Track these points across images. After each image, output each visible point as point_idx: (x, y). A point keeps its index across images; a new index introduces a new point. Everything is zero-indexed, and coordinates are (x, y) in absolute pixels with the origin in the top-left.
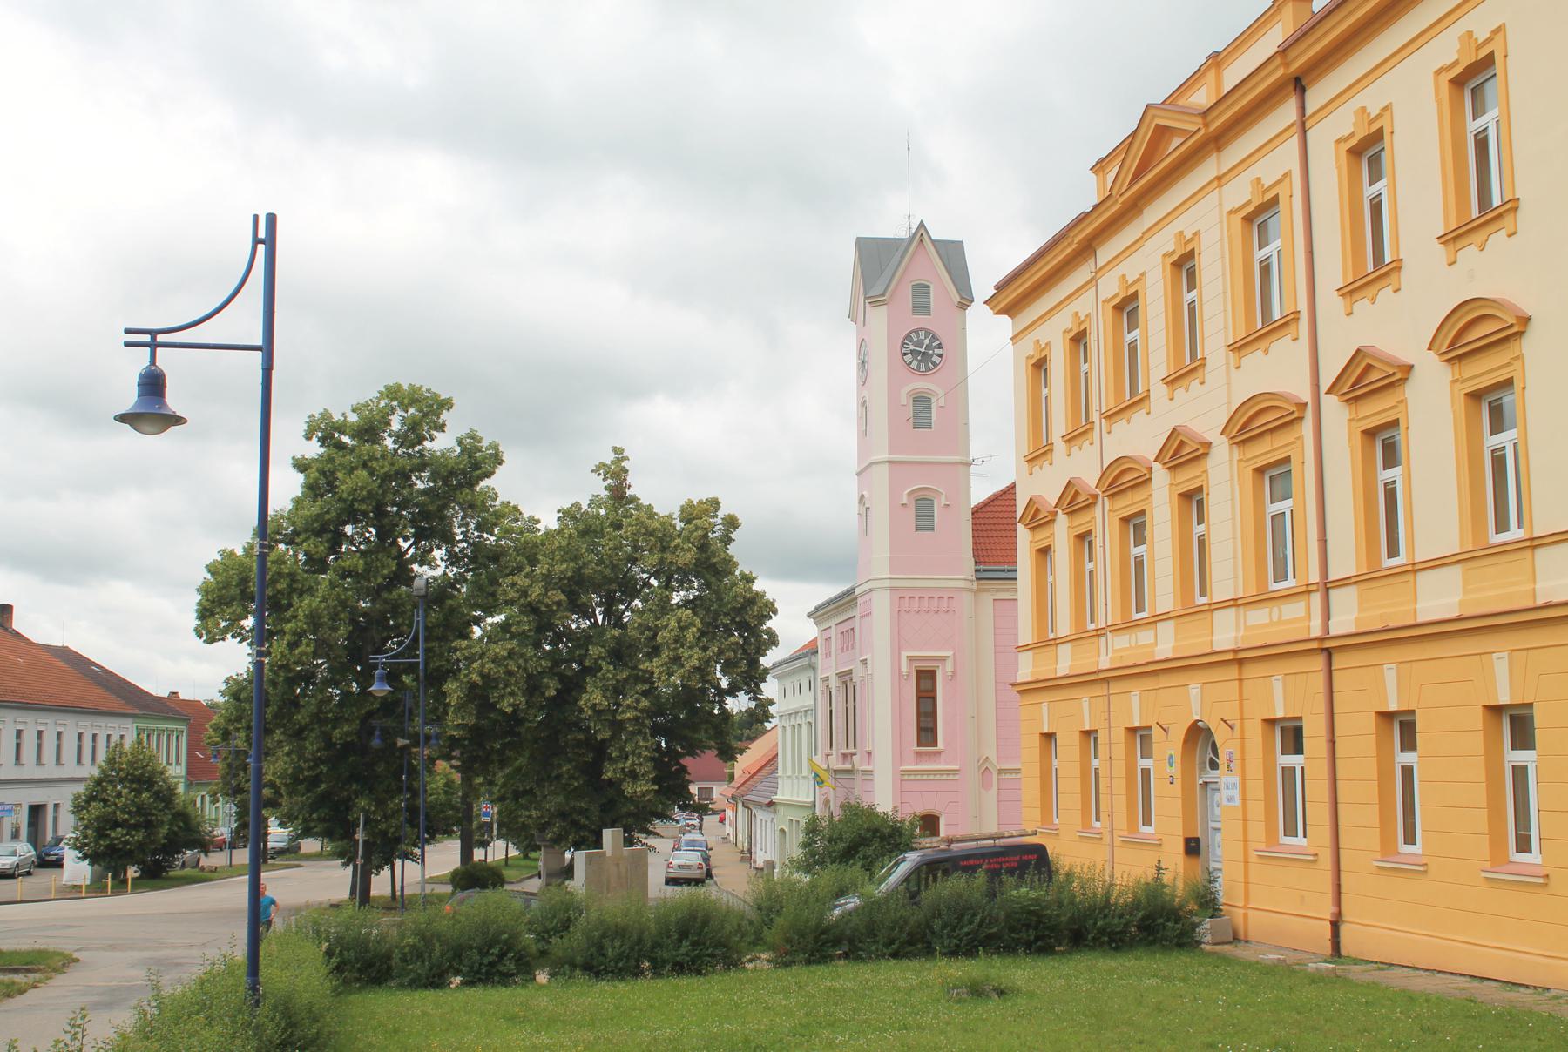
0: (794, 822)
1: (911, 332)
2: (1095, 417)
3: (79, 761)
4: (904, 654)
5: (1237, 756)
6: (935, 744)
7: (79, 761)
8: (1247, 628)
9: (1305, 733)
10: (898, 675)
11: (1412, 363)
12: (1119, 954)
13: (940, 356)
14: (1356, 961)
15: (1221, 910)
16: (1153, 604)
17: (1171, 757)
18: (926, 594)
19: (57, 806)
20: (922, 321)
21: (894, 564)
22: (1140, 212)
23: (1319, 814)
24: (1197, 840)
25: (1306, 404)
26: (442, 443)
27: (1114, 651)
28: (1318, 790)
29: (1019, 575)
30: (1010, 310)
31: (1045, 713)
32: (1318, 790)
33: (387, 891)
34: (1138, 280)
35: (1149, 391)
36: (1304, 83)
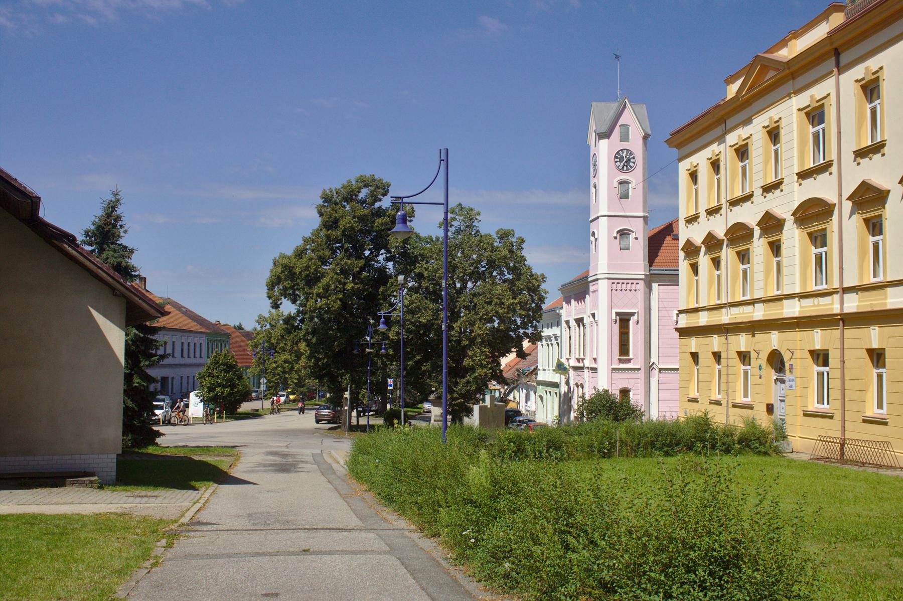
0: (548, 393)
1: (619, 151)
2: (723, 201)
3: (182, 356)
4: (614, 311)
5: (613, 323)
6: (628, 354)
7: (182, 356)
8: (801, 307)
9: (830, 357)
10: (612, 322)
11: (889, 189)
12: (139, 487)
13: (634, 163)
14: (856, 463)
15: (159, 434)
16: (752, 292)
17: (760, 366)
18: (630, 281)
19: (173, 378)
20: (625, 145)
21: (609, 266)
22: (751, 104)
23: (835, 394)
24: (772, 405)
25: (835, 204)
26: (385, 203)
27: (731, 315)
28: (835, 384)
29: (680, 273)
30: (679, 146)
31: (693, 344)
32: (835, 384)
33: (356, 424)
34: (748, 138)
35: (753, 192)
36: (839, 51)
